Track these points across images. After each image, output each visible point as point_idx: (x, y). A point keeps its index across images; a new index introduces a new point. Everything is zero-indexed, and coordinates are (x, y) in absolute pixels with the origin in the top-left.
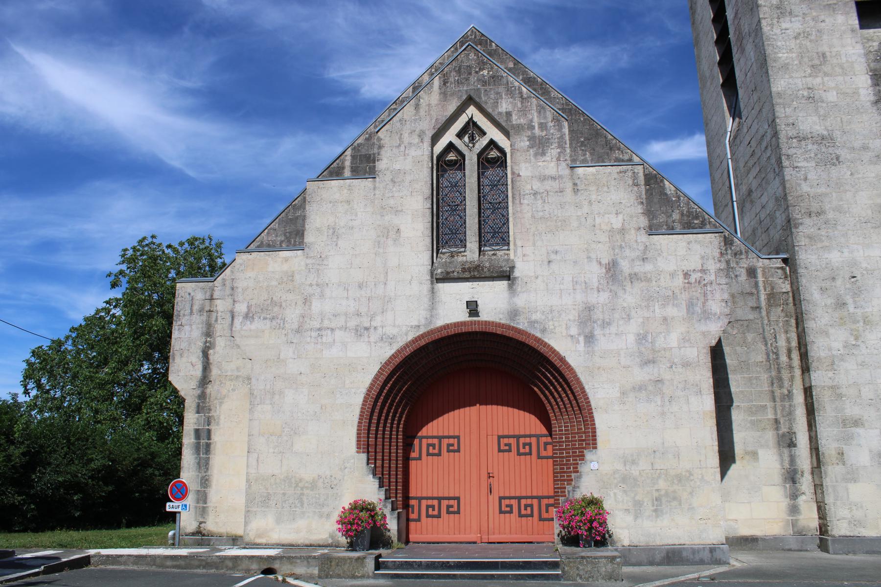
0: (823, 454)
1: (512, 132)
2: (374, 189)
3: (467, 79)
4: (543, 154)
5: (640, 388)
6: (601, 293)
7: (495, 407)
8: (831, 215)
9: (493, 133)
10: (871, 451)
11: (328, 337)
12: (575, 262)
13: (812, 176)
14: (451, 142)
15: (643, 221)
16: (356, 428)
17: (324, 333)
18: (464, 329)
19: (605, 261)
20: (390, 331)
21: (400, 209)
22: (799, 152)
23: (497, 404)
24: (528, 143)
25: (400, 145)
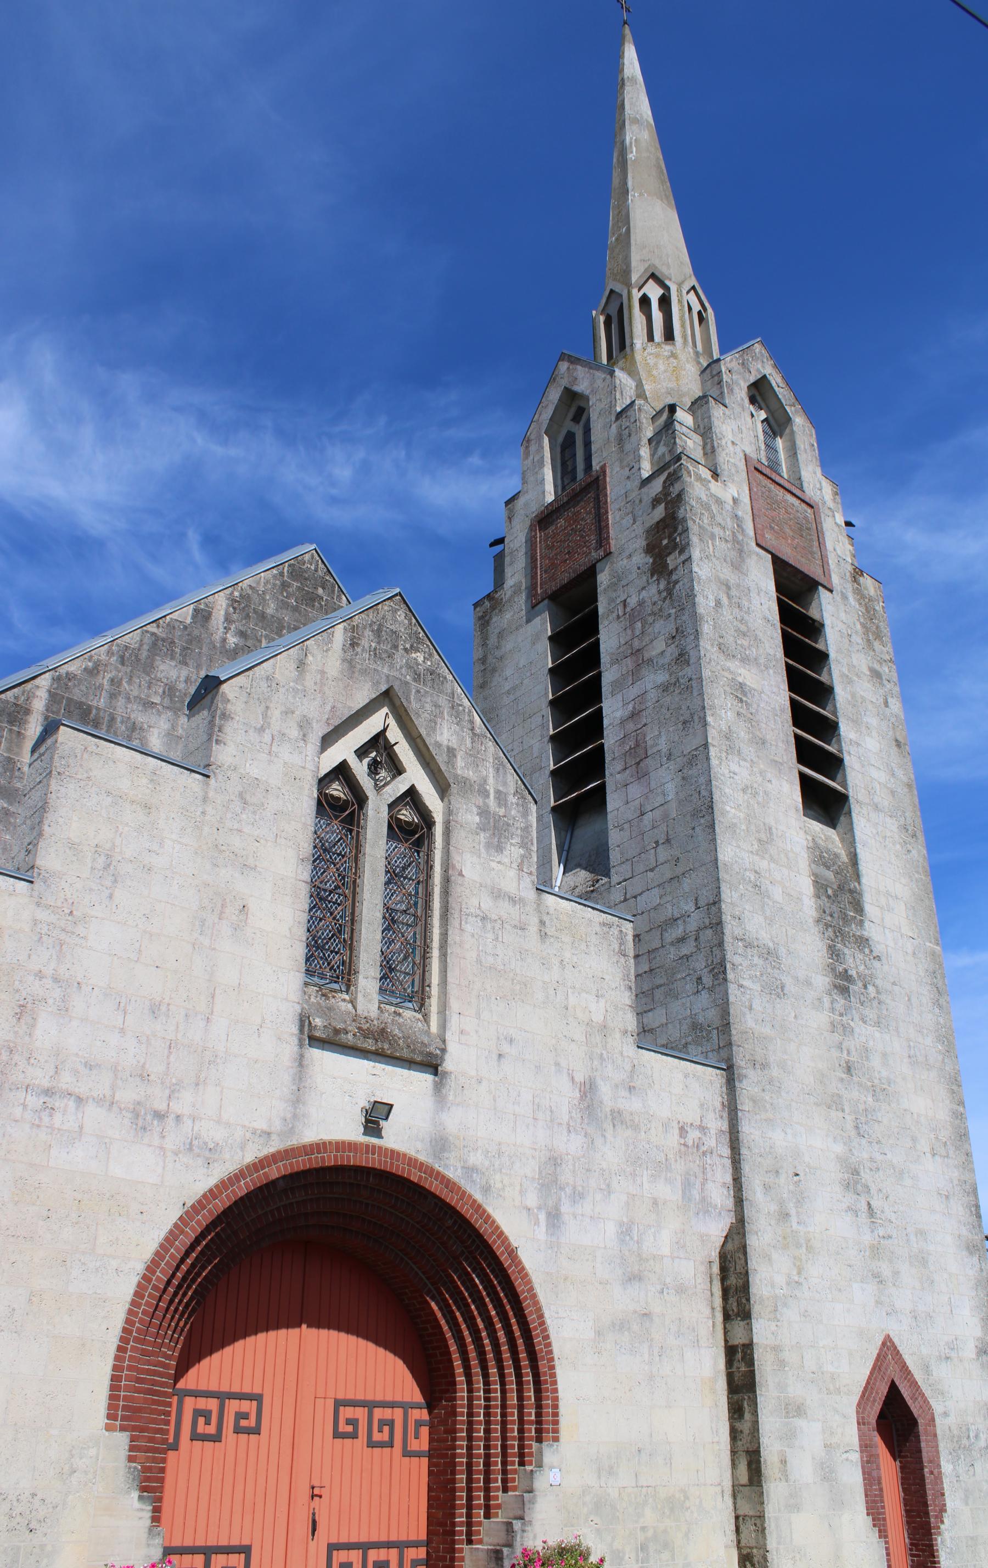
0: (765, 1461)
1: (454, 788)
2: (205, 799)
3: (390, 656)
4: (499, 849)
5: (621, 1326)
6: (573, 1135)
7: (333, 1333)
8: (775, 1072)
9: (414, 775)
10: (813, 1458)
11: (66, 1117)
12: (538, 1068)
13: (757, 1005)
14: (345, 760)
15: (630, 1021)
16: (110, 1362)
17: (58, 1103)
18: (353, 1160)
19: (579, 1078)
20: (212, 1133)
21: (251, 862)
22: (745, 963)
23: (339, 1329)
24: (477, 819)
25: (261, 730)
